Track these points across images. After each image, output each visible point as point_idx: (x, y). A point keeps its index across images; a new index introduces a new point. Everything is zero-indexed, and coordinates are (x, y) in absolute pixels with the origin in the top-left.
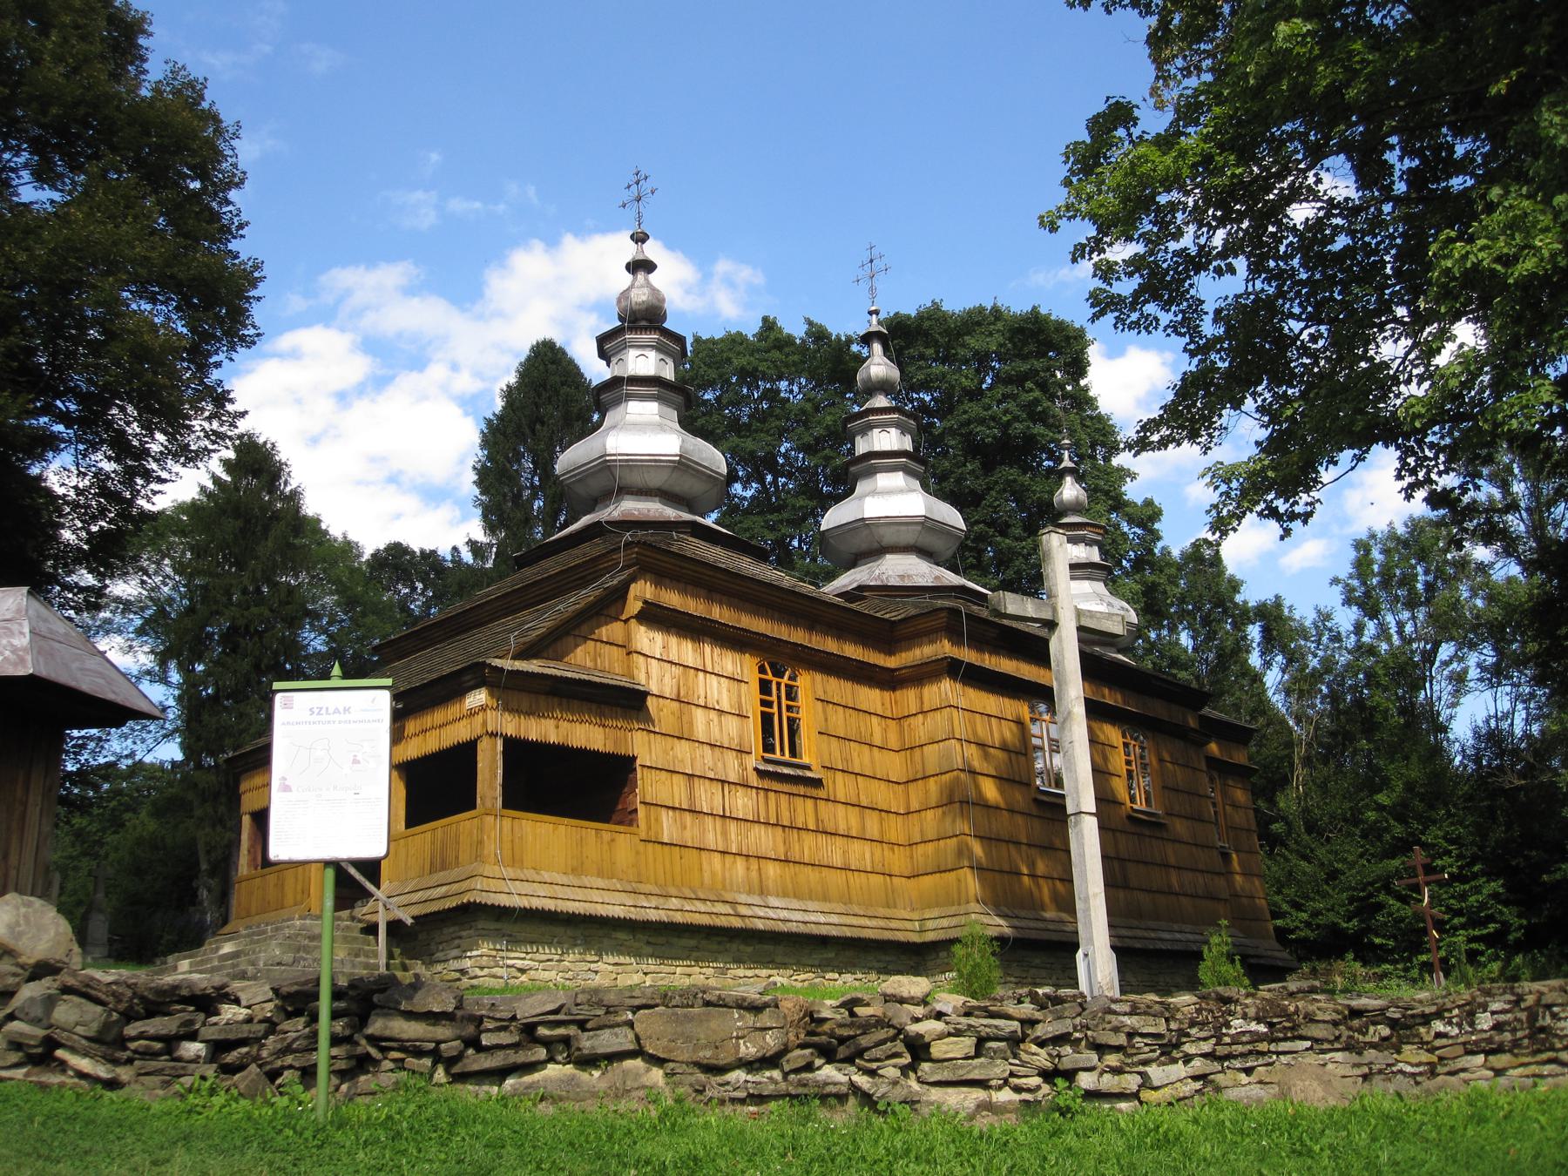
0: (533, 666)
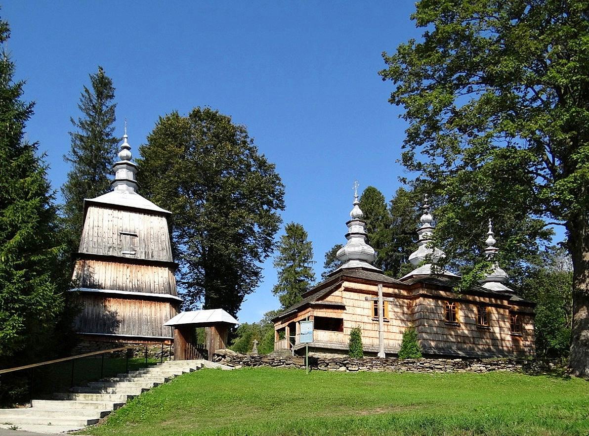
0: (320, 302)
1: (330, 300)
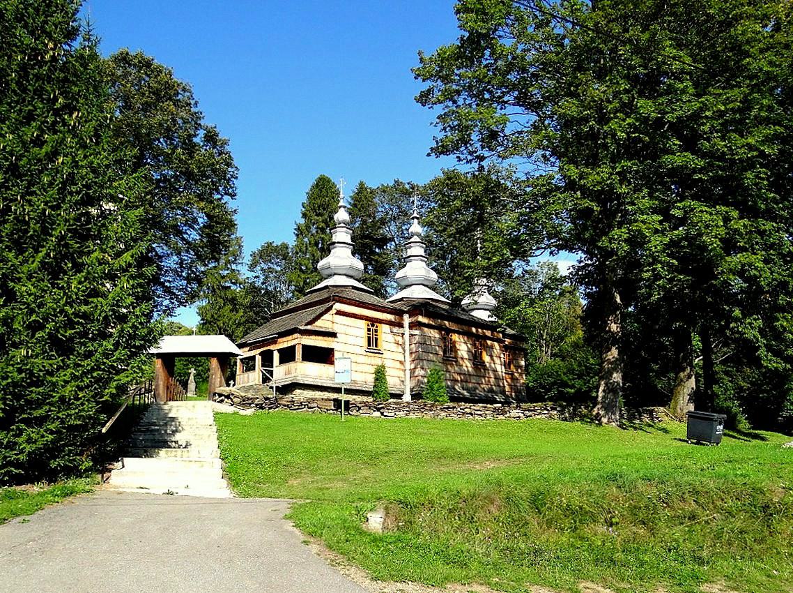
0: (309, 327)
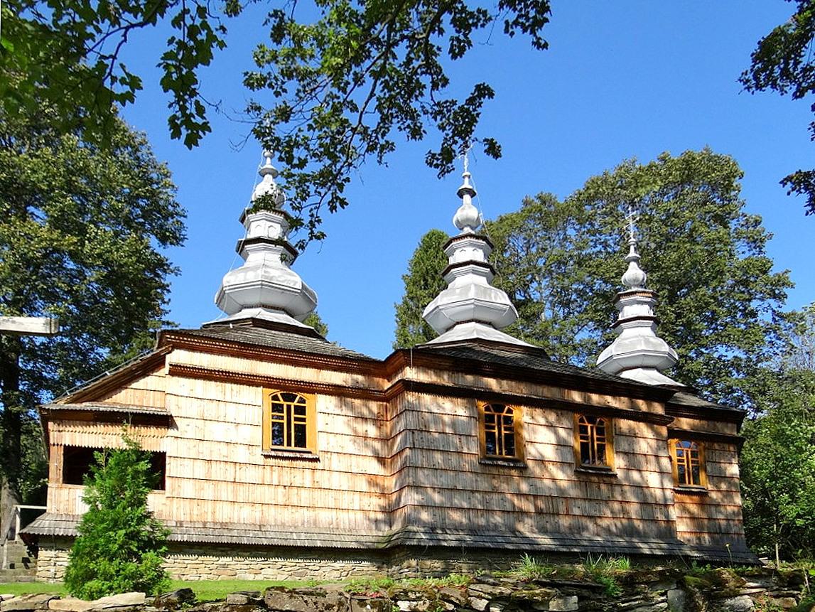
1: (125, 399)
